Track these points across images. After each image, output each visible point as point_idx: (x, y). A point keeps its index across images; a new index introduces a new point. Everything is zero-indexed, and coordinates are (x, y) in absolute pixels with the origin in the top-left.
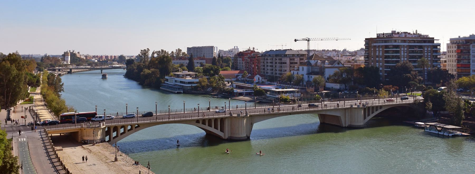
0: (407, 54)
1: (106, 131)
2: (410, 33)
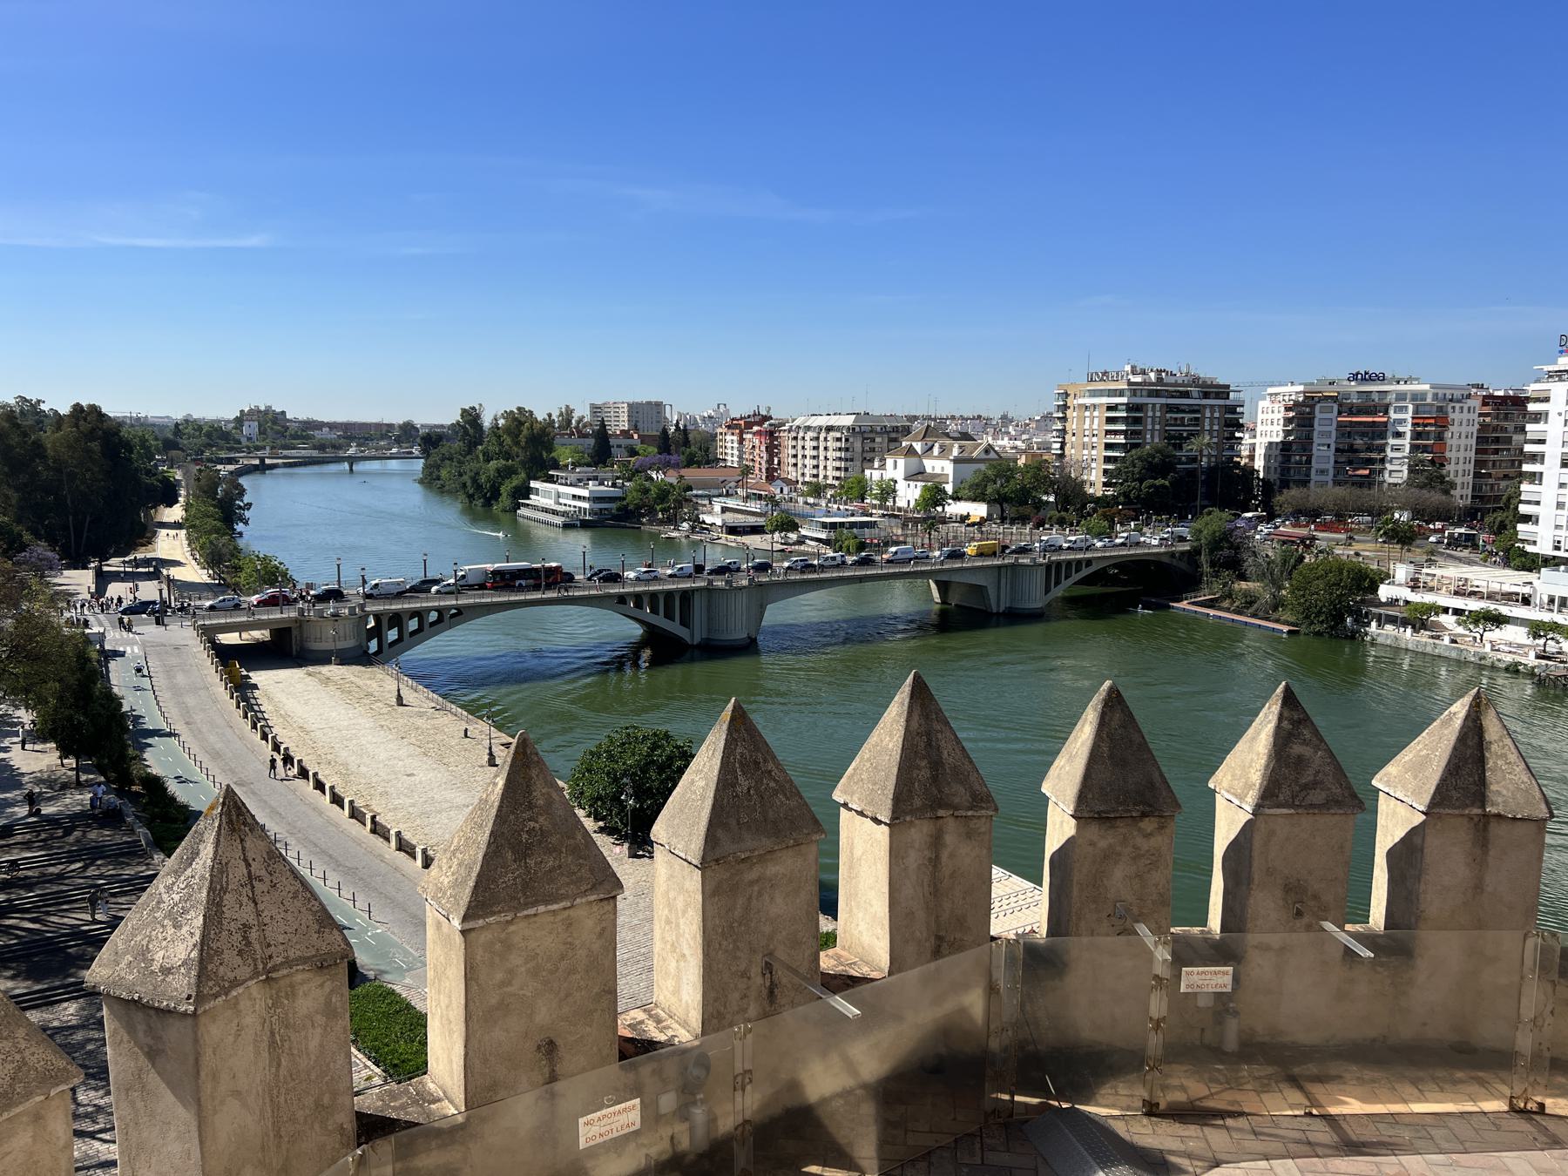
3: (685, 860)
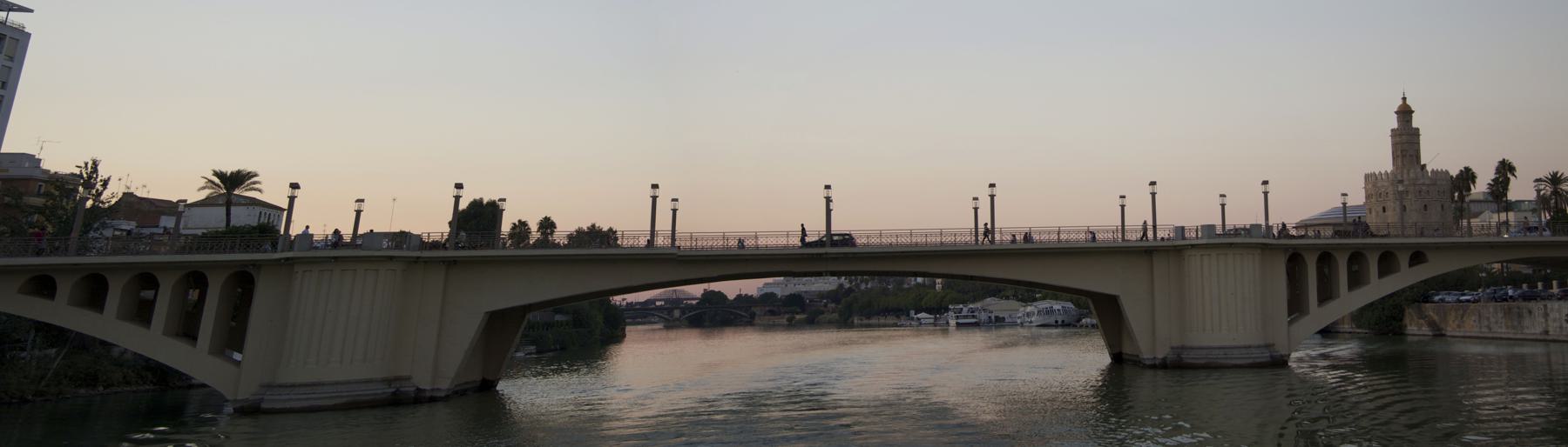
1: (463, 211)
2: (481, 199)
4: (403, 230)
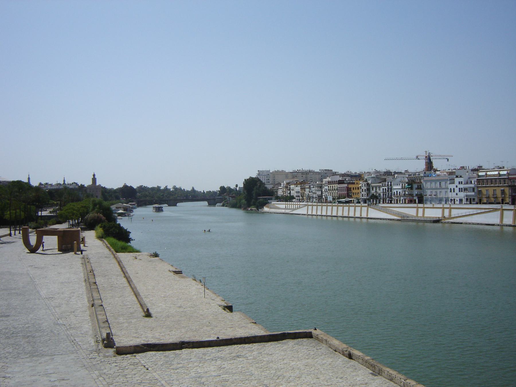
0: (203, 193)
2: (92, 178)
3: (407, 367)
4: (132, 186)
